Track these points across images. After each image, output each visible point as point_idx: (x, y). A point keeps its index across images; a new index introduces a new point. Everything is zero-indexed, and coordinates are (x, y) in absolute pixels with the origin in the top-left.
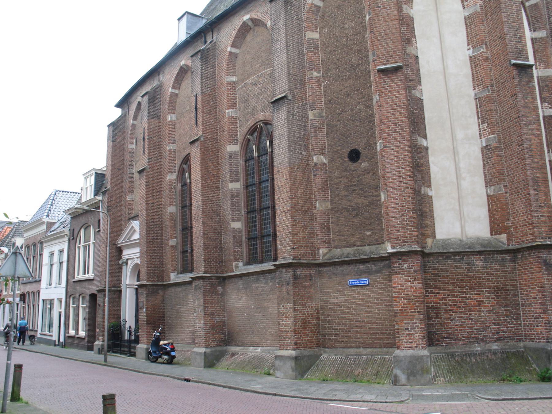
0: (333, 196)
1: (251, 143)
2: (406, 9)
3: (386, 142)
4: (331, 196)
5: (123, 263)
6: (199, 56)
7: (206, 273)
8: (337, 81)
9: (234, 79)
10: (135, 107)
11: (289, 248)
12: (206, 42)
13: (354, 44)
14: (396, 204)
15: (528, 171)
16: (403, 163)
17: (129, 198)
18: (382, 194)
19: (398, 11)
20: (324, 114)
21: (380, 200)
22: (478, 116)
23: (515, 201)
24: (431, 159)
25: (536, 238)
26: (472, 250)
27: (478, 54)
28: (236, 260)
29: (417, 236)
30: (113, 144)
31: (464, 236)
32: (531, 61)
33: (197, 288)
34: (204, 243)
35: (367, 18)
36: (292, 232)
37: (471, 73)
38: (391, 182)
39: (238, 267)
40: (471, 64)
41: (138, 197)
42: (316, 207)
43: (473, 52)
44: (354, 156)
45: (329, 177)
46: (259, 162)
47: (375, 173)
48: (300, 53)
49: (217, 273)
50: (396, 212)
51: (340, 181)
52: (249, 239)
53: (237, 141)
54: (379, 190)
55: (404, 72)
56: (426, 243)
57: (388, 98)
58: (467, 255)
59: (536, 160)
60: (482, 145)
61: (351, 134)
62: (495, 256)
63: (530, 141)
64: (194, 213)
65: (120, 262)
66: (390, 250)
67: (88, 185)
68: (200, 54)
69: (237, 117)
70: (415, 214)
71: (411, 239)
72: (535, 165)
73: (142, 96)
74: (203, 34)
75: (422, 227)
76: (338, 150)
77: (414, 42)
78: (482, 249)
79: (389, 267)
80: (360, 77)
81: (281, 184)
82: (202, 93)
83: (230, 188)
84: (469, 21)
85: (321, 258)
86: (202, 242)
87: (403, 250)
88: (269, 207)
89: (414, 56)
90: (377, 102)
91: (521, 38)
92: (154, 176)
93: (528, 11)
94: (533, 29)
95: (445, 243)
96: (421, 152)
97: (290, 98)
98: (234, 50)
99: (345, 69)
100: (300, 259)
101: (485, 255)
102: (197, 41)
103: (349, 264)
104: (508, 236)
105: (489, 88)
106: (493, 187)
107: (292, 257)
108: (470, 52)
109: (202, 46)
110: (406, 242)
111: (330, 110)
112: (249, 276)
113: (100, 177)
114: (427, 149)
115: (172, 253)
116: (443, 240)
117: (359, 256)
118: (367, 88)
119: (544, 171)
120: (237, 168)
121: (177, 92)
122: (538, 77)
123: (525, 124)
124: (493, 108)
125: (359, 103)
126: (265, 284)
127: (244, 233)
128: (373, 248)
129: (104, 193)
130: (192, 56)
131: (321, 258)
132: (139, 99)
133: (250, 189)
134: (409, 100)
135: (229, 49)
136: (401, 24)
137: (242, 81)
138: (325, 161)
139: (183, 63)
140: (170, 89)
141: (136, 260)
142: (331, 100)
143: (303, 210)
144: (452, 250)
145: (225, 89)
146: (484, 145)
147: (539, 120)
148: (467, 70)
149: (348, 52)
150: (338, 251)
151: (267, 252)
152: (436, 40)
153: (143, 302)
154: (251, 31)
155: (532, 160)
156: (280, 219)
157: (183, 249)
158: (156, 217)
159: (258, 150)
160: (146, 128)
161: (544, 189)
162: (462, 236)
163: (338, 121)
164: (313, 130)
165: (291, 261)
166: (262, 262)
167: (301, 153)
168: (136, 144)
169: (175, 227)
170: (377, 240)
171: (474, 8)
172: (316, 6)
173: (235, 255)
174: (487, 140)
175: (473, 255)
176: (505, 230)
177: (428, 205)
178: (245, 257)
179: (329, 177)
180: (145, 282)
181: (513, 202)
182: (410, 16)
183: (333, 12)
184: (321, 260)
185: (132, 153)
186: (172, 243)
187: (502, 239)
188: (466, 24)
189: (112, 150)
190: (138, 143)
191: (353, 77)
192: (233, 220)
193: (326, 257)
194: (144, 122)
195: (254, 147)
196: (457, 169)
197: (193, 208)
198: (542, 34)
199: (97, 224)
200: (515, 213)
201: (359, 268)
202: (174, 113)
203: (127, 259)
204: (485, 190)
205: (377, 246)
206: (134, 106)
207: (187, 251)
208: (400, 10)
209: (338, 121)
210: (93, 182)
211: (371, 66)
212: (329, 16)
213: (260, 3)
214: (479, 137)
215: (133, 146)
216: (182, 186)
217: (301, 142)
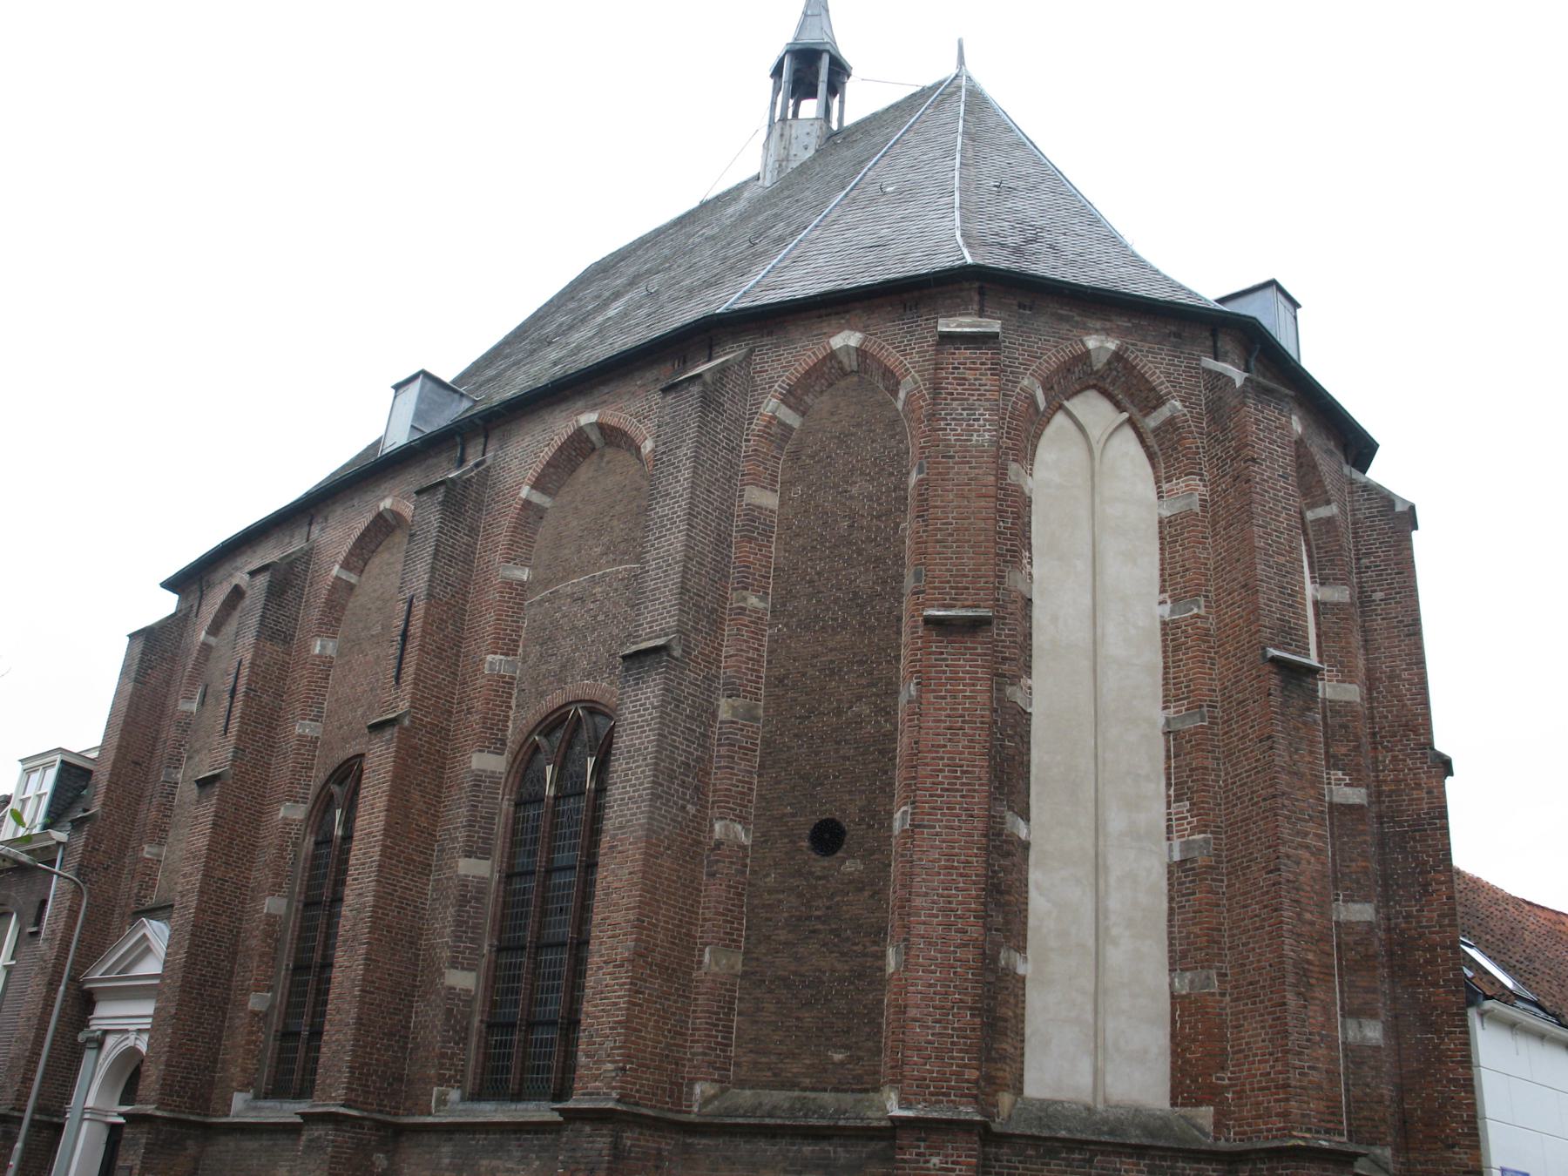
0: (753, 939)
1: (541, 756)
2: (1017, 475)
4: (747, 937)
5: (89, 1040)
6: (440, 497)
7: (350, 1107)
8: (807, 628)
10: (222, 597)
11: (610, 1066)
12: (462, 461)
13: (869, 540)
14: (930, 985)
16: (961, 875)
17: (148, 851)
18: (891, 952)
20: (761, 712)
21: (882, 969)
22: (1169, 779)
23: (1245, 1018)
24: (1034, 876)
25: (1293, 1128)
26: (1119, 1140)
27: (1185, 619)
28: (442, 1080)
29: (976, 1082)
30: (135, 688)
31: (1100, 1099)
33: (314, 1146)
34: (359, 1018)
35: (914, 478)
36: (625, 1024)
38: (924, 923)
39: (445, 1102)
40: (1164, 641)
41: (181, 851)
42: (700, 962)
43: (1172, 612)
44: (828, 837)
45: (750, 884)
46: (556, 814)
47: (878, 894)
48: (722, 540)
49: (380, 1112)
50: (928, 1006)
51: (780, 901)
52: (490, 1026)
53: (504, 743)
55: (994, 633)
56: (995, 1105)
57: (944, 698)
58: (1102, 1153)
59: (1308, 916)
60: (1171, 857)
61: (827, 777)
62: (1180, 1164)
63: (1298, 863)
64: (344, 926)
65: (81, 1037)
66: (897, 1112)
67: (30, 793)
68: (442, 489)
69: (513, 678)
70: (977, 1020)
71: (959, 1088)
72: (1305, 929)
73: (253, 574)
74: (458, 439)
75: (989, 1059)
76: (784, 815)
78: (1146, 1141)
79: (887, 1159)
80: (872, 629)
81: (616, 885)
82: (430, 595)
83: (461, 872)
84: (1170, 533)
85: (695, 1109)
86: (354, 1012)
87: (935, 1115)
88: (564, 944)
89: (1023, 597)
91: (1293, 596)
92: (238, 800)
93: (1310, 532)
95: (1048, 1111)
96: (1008, 854)
97: (677, 653)
98: (537, 498)
99: (836, 601)
100: (637, 1104)
101: (1153, 1158)
103: (774, 1136)
104: (1217, 1113)
106: (1188, 975)
107: (614, 1095)
108: (1166, 610)
110: (944, 1094)
111: (779, 705)
112: (474, 1132)
113: (73, 776)
114: (1026, 846)
115: (251, 1033)
116: (1042, 1101)
117: (806, 1116)
118: (889, 662)
120: (490, 818)
121: (353, 579)
123: (1289, 818)
124: (1210, 763)
125: (859, 699)
126: (519, 1162)
127: (478, 1006)
128: (848, 1098)
129: (77, 825)
130: (419, 493)
131: (695, 1109)
132: (241, 578)
133: (517, 885)
135: (525, 492)
136: (1000, 511)
137: (547, 583)
138: (745, 839)
139: (386, 504)
140: (337, 567)
141: (132, 1036)
142: (786, 676)
143: (663, 965)
144: (1063, 1134)
145: (494, 595)
146: (1177, 857)
148: (1153, 656)
149: (850, 557)
150: (746, 1097)
151: (538, 1070)
152: (1082, 566)
153: (131, 1168)
154: (594, 457)
155: (1299, 914)
156: (598, 982)
157: (285, 1025)
158: (224, 920)
159: (559, 781)
160: (246, 663)
161: (1322, 997)
162: (1095, 1099)
163: (796, 736)
164: (723, 751)
165: (610, 1105)
166: (518, 1097)
167: (684, 807)
168: (203, 703)
169: (274, 959)
170: (858, 1079)
172: (782, 424)
173: (442, 1066)
174: (1186, 846)
175: (1119, 1154)
176: (1210, 1095)
177: (1012, 1000)
178: (470, 1076)
179: (750, 884)
180: (150, 1109)
181: (1238, 1019)
184: (694, 1113)
185: (186, 725)
186: (256, 1002)
187: (1200, 1121)
188: (1162, 538)
189: (130, 707)
190: (210, 700)
191: (853, 627)
192: (454, 964)
193: (710, 1108)
194: (240, 646)
195: (549, 769)
196: (1100, 913)
197: (345, 911)
198: (1338, 594)
199: (33, 911)
200: (1241, 1051)
201: (799, 1151)
203: (106, 1032)
204: (1167, 980)
205: (859, 1096)
206: (217, 597)
207: (299, 1034)
208: (1001, 473)
209: (796, 736)
210: (48, 785)
211: (907, 603)
212: (812, 457)
214: (1164, 835)
215: (194, 707)
216: (317, 844)
217: (684, 779)
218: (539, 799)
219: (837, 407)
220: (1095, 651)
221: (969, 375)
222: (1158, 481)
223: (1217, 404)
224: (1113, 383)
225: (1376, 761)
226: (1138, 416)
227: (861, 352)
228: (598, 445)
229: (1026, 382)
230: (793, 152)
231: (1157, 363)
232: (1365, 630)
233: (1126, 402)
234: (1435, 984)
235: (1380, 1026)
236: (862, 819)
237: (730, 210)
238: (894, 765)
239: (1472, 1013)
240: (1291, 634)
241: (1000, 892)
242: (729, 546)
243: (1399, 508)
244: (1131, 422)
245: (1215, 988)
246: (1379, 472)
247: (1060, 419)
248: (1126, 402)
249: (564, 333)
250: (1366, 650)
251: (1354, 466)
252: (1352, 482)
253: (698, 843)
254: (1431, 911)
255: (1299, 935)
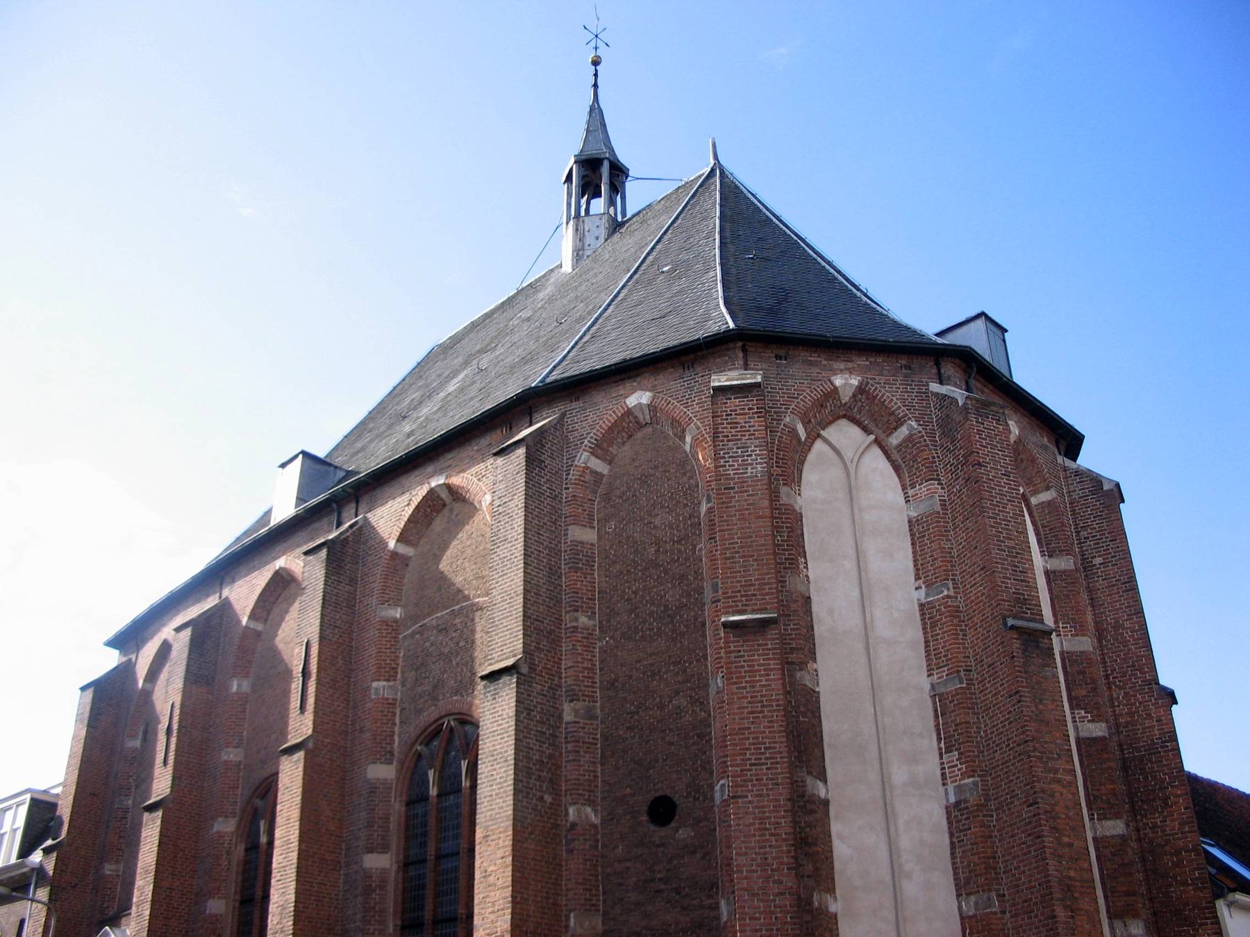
1: (424, 762)
2: (788, 495)
3: (737, 786)
4: (605, 901)
9: (397, 613)
14: (757, 931)
15: (1050, 862)
16: (773, 835)
18: (723, 903)
19: (771, 501)
21: (718, 918)
22: (939, 734)
24: (836, 827)
27: (938, 600)
32: (1049, 620)
35: (704, 508)
37: (923, 640)
38: (746, 878)
42: (567, 927)
43: (927, 595)
44: (662, 811)
46: (439, 811)
48: (553, 572)
53: (392, 753)
54: (717, 893)
57: (744, 688)
59: (1066, 839)
60: (947, 800)
61: (657, 761)
69: (395, 700)
73: (178, 630)
74: (335, 506)
76: (625, 796)
77: (801, 566)
89: (803, 596)
90: (718, 693)
91: (1024, 575)
93: (1035, 514)
94: (1049, 551)
96: (813, 811)
102: (319, 519)
105: (962, 674)
106: (973, 898)
109: (330, 531)
114: (826, 803)
118: (698, 661)
119: (1086, 865)
120: (387, 818)
121: (259, 627)
122: (1062, 653)
125: (677, 693)
134: (789, 693)
137: (415, 618)
142: (616, 680)
146: (952, 799)
147: (1070, 750)
152: (849, 565)
154: (446, 511)
160: (177, 706)
163: (628, 728)
164: (570, 747)
167: (542, 798)
171: (927, 503)
172: (594, 473)
174: (959, 789)
179: (603, 857)
182: (794, 510)
183: (629, 489)
195: (431, 773)
198: (1064, 563)
202: (247, 676)
206: (149, 651)
208: (774, 495)
213: (471, 453)
216: (247, 850)
218: (425, 798)
219: (637, 454)
220: (866, 634)
221: (740, 419)
222: (904, 488)
223: (947, 420)
224: (860, 411)
225: (1111, 699)
226: (882, 436)
227: (652, 407)
228: (448, 502)
229: (788, 419)
230: (587, 243)
231: (892, 389)
232: (1090, 590)
233: (871, 426)
234: (1185, 883)
235: (1141, 924)
236: (689, 794)
237: (541, 295)
238: (711, 746)
239: (1220, 904)
240: (1026, 603)
241: (807, 844)
242: (560, 577)
243: (1106, 487)
244: (877, 442)
245: (996, 908)
246: (1087, 459)
247: (819, 446)
248: (871, 426)
249: (415, 409)
250: (1093, 606)
251: (1066, 456)
252: (1065, 469)
253: (556, 826)
254: (1172, 821)
255: (1061, 857)
